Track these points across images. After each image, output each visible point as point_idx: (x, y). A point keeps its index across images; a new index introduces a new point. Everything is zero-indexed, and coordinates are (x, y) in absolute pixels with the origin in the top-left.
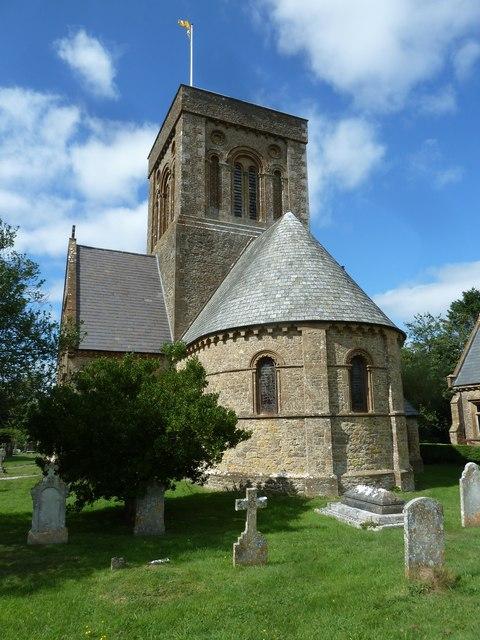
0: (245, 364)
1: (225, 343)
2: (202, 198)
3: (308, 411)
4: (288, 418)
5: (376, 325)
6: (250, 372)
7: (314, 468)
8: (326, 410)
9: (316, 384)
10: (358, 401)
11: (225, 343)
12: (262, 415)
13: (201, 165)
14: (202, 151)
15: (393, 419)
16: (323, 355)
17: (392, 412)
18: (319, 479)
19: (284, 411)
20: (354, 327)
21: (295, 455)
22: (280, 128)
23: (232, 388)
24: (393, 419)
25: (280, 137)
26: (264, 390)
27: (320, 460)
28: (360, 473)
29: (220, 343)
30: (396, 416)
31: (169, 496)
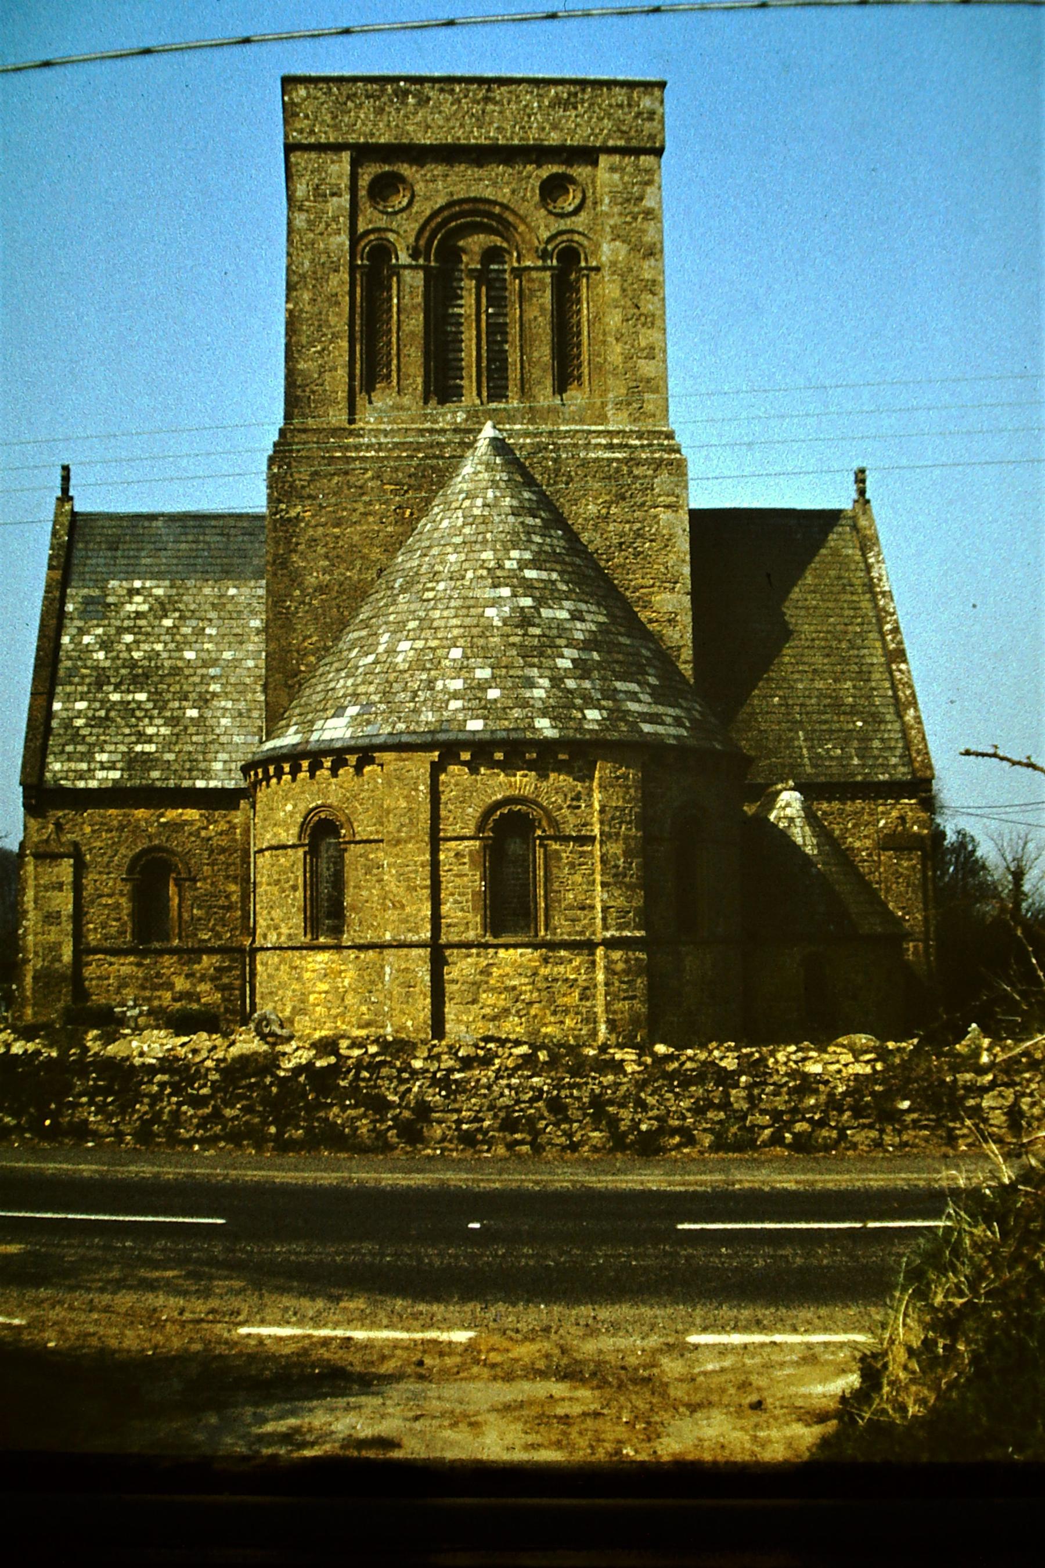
8: (426, 935)
19: (346, 939)
22: (575, 128)
23: (277, 882)
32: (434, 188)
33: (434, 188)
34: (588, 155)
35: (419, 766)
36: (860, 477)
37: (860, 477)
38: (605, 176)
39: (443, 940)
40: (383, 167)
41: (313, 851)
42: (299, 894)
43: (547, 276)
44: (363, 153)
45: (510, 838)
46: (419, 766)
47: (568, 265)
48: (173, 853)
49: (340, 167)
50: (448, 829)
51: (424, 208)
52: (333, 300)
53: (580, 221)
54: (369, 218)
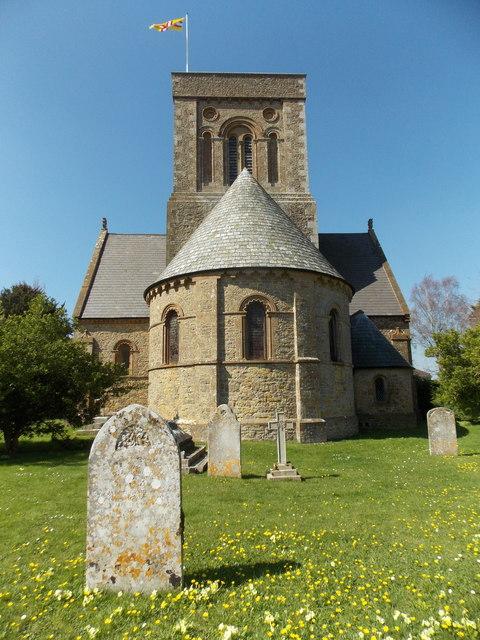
0: (236, 310)
1: (177, 290)
2: (193, 176)
3: (198, 360)
4: (185, 367)
5: (261, 268)
6: (240, 317)
7: (198, 416)
8: (214, 357)
9: (206, 332)
10: (253, 348)
11: (177, 290)
12: (171, 365)
13: (193, 144)
14: (193, 131)
15: (297, 366)
16: (214, 304)
17: (297, 359)
18: (201, 426)
19: (182, 360)
20: (249, 273)
21: (189, 402)
22: (273, 90)
24: (297, 366)
25: (274, 100)
26: (172, 342)
27: (205, 407)
28: (250, 421)
29: (172, 291)
30: (300, 362)
31: (24, 443)
32: (227, 114)
33: (227, 114)
34: (280, 101)
35: (213, 280)
36: (370, 223)
37: (370, 223)
38: (287, 108)
39: (227, 360)
40: (207, 106)
41: (168, 325)
42: (161, 344)
43: (265, 144)
44: (200, 100)
45: (253, 314)
46: (213, 280)
47: (272, 139)
48: (129, 342)
49: (192, 106)
50: (228, 309)
51: (223, 119)
52: (190, 149)
53: (277, 124)
54: (205, 123)
